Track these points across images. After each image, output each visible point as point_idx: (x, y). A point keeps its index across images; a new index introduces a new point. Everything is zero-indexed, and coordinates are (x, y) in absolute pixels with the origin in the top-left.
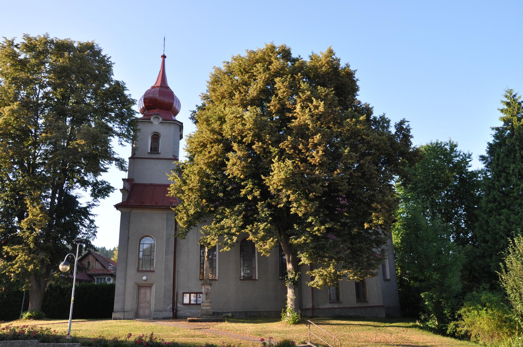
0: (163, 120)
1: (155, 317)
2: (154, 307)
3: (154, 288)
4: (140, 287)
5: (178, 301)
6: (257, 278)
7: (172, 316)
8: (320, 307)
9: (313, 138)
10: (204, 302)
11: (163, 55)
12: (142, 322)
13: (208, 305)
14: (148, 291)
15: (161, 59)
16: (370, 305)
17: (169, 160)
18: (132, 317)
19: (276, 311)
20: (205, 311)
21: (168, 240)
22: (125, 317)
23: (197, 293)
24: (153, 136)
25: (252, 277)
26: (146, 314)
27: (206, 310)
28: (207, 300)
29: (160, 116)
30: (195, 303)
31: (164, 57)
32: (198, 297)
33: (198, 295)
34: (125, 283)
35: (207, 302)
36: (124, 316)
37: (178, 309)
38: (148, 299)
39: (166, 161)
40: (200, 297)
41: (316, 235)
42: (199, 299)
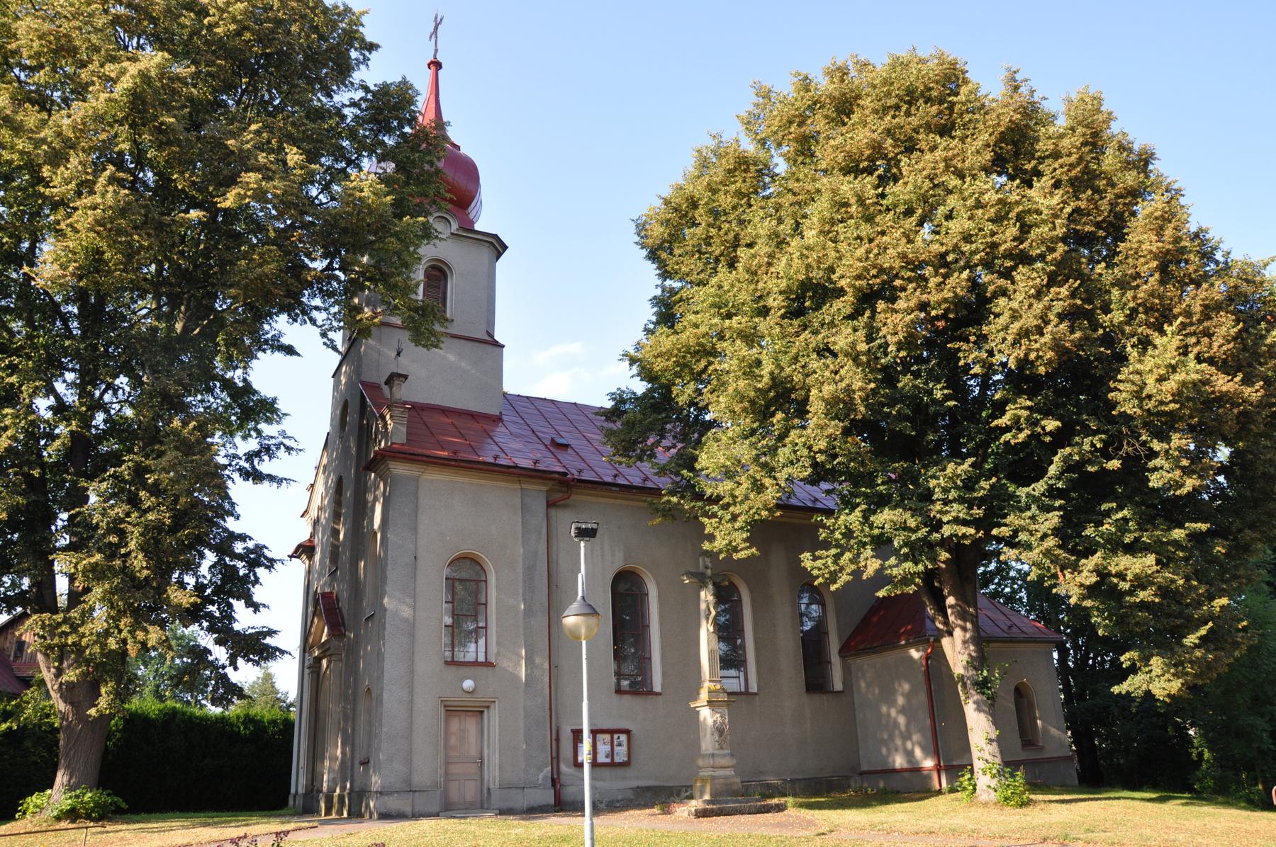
0: (460, 228)
1: (504, 806)
2: (497, 774)
3: (494, 718)
4: (451, 710)
5: (562, 756)
6: (657, 687)
7: (552, 801)
8: (955, 763)
9: (983, 338)
10: (718, 755)
11: (431, 58)
12: (807, 811)
13: (727, 765)
14: (471, 724)
15: (429, 73)
16: (1047, 756)
17: (477, 344)
18: (436, 809)
19: (805, 779)
20: (721, 781)
21: (530, 569)
22: (417, 809)
23: (611, 732)
24: (431, 266)
25: (643, 683)
26: (468, 798)
27: (726, 778)
28: (722, 748)
29: (454, 216)
30: (608, 760)
31: (436, 65)
32: (615, 743)
33: (616, 736)
34: (412, 702)
35: (724, 755)
36: (413, 806)
37: (563, 779)
38: (473, 751)
39: (468, 344)
40: (620, 745)
41: (235, 569)
42: (617, 749)
